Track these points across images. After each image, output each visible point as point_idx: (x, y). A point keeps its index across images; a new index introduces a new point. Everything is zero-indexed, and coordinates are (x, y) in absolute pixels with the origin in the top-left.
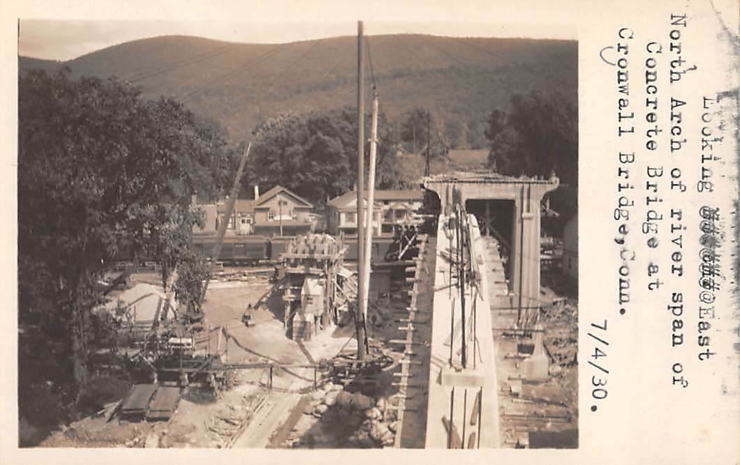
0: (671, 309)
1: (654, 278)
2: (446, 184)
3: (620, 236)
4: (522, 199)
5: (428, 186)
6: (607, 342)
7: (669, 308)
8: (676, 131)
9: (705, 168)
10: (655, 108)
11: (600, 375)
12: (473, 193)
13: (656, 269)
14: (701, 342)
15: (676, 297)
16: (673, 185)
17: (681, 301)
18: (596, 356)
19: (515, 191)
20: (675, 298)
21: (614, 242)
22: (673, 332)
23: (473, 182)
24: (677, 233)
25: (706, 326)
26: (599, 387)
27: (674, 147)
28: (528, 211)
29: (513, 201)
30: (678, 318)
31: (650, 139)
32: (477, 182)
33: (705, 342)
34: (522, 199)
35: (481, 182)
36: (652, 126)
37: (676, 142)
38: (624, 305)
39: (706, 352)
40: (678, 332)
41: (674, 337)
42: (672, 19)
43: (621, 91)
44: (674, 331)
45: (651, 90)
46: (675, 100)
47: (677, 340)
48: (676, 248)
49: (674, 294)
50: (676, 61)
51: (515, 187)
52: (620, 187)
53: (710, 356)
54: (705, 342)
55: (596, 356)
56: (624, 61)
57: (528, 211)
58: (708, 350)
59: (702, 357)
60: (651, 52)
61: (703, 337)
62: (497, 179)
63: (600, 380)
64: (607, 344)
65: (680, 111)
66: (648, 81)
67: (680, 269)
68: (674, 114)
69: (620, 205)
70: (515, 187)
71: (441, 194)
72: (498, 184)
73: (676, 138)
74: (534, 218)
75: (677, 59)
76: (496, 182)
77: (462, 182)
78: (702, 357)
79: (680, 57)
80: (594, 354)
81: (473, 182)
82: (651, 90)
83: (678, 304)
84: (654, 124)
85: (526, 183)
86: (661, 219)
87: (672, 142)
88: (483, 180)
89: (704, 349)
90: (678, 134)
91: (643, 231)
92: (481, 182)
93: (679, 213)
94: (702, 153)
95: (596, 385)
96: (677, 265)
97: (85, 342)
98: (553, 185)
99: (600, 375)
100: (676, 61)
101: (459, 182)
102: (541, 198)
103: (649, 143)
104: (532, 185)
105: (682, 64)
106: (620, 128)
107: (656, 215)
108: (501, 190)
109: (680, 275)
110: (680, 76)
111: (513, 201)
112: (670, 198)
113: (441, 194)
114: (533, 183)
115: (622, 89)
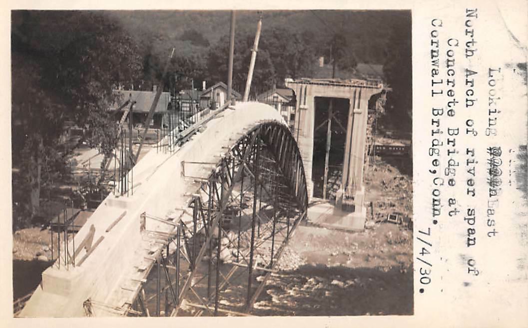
0: (467, 221)
1: (453, 207)
2: (301, 84)
3: (433, 168)
4: (355, 97)
5: (288, 85)
6: (431, 264)
7: (465, 219)
8: (470, 93)
9: (491, 119)
10: (453, 86)
11: (425, 267)
12: (319, 92)
13: (454, 202)
14: (489, 224)
15: (470, 212)
16: (468, 131)
17: (474, 215)
18: (423, 253)
19: (350, 92)
20: (470, 213)
21: (429, 172)
22: (468, 237)
23: (321, 84)
24: (471, 166)
25: (493, 212)
26: (425, 275)
27: (468, 104)
28: (359, 107)
29: (348, 100)
30: (471, 227)
31: (450, 108)
32: (323, 84)
33: (492, 224)
34: (355, 97)
35: (326, 84)
36: (451, 99)
37: (470, 100)
38: (436, 218)
39: (493, 231)
40: (472, 237)
41: (469, 239)
42: (467, 12)
43: (433, 65)
44: (469, 236)
45: (451, 73)
46: (469, 71)
47: (471, 242)
48: (470, 176)
49: (470, 210)
50: (470, 42)
51: (350, 89)
52: (433, 132)
53: (496, 234)
54: (492, 224)
55: (423, 253)
56: (436, 141)
57: (359, 107)
58: (494, 230)
59: (490, 234)
60: (451, 45)
61: (491, 220)
62: (339, 83)
63: (426, 271)
64: (431, 266)
65: (473, 78)
66: (448, 66)
67: (473, 191)
68: (468, 80)
69: (433, 145)
70: (350, 89)
71: (297, 91)
72: (338, 87)
73: (470, 98)
74: (363, 113)
75: (471, 41)
76: (337, 85)
77: (312, 83)
78: (490, 234)
79: (473, 40)
80: (422, 252)
81: (321, 84)
82: (451, 73)
83: (472, 217)
84: (453, 98)
85: (359, 87)
86: (458, 165)
87: (467, 100)
88: (328, 83)
89: (491, 229)
90: (471, 95)
91: (445, 173)
92: (326, 84)
93: (473, 152)
94: (489, 108)
95: (423, 274)
96: (471, 188)
97: (205, 243)
98: (378, 90)
99: (425, 267)
100: (470, 42)
101: (310, 83)
102: (369, 99)
103: (449, 111)
104: (362, 89)
105: (474, 44)
106: (433, 91)
107: (454, 162)
108: (340, 91)
109: (473, 195)
110: (473, 53)
111: (348, 100)
112: (463, 141)
113: (297, 91)
114: (364, 87)
115: (433, 63)
